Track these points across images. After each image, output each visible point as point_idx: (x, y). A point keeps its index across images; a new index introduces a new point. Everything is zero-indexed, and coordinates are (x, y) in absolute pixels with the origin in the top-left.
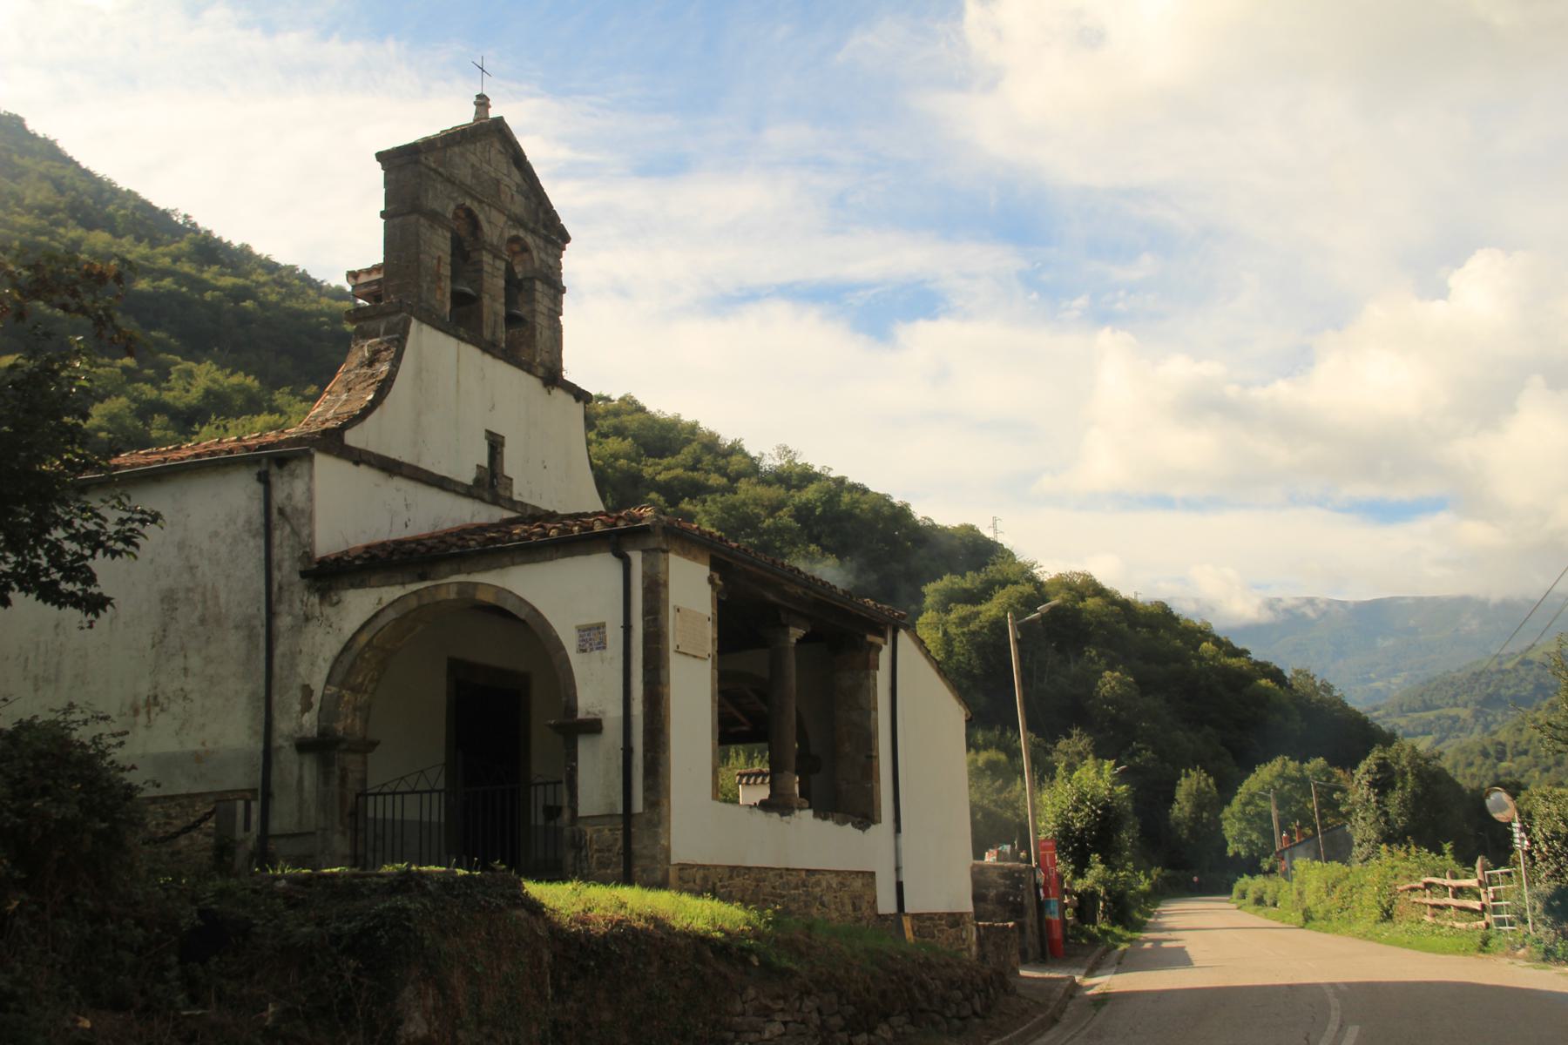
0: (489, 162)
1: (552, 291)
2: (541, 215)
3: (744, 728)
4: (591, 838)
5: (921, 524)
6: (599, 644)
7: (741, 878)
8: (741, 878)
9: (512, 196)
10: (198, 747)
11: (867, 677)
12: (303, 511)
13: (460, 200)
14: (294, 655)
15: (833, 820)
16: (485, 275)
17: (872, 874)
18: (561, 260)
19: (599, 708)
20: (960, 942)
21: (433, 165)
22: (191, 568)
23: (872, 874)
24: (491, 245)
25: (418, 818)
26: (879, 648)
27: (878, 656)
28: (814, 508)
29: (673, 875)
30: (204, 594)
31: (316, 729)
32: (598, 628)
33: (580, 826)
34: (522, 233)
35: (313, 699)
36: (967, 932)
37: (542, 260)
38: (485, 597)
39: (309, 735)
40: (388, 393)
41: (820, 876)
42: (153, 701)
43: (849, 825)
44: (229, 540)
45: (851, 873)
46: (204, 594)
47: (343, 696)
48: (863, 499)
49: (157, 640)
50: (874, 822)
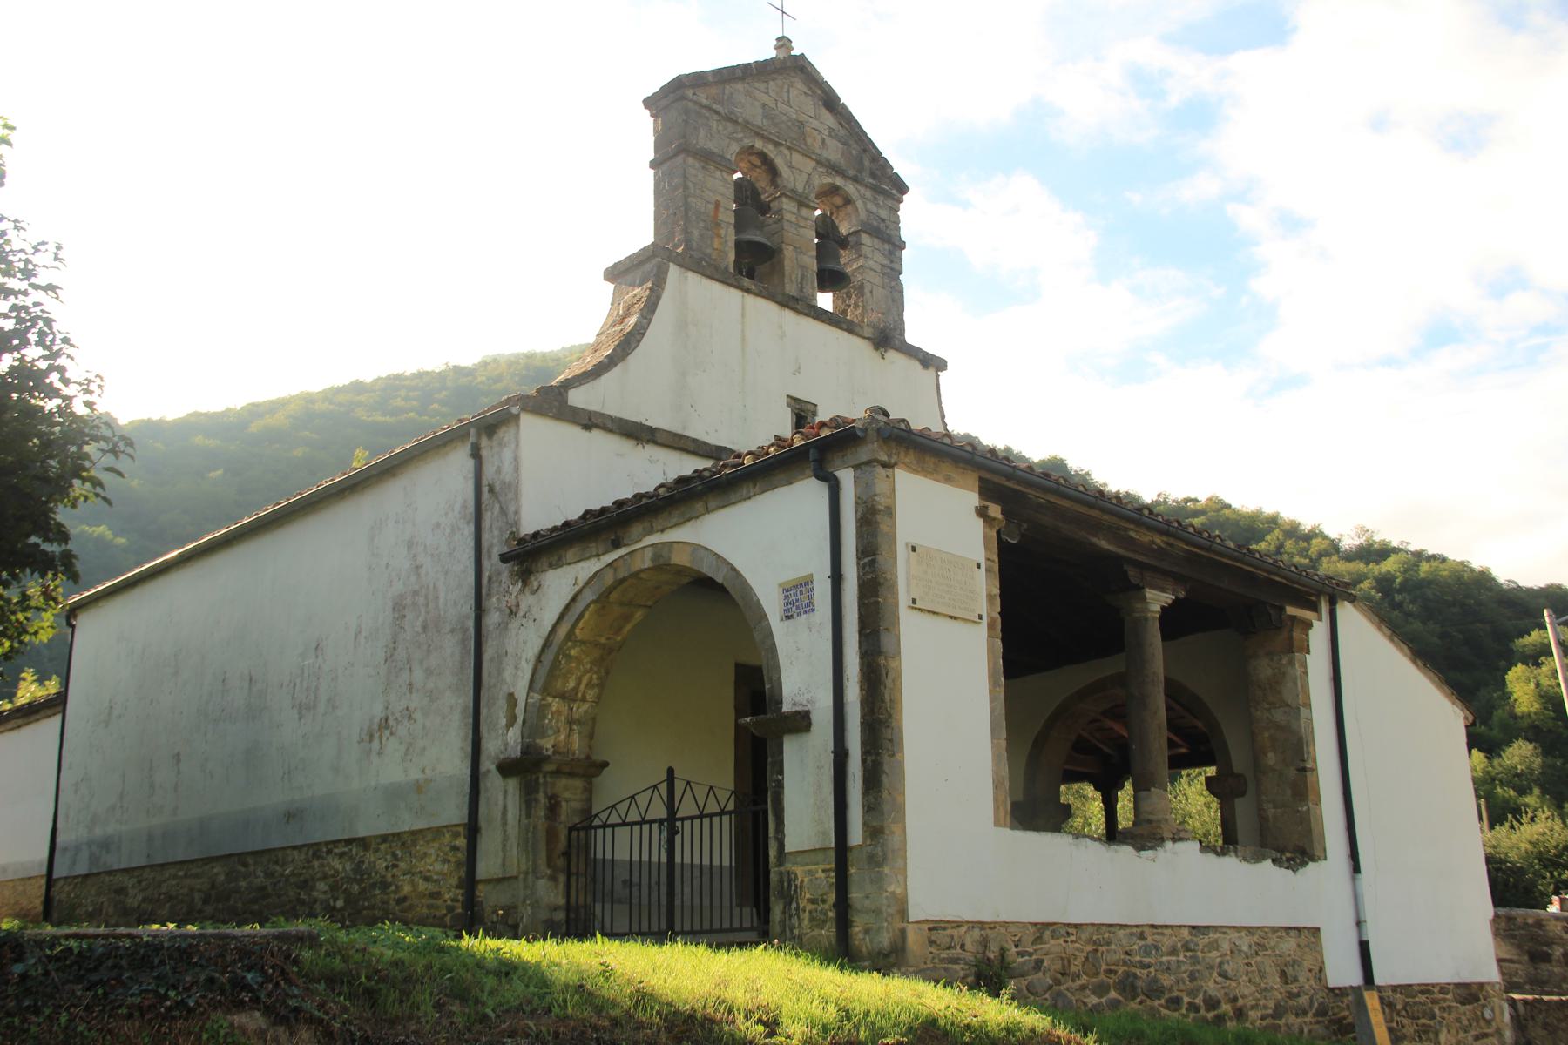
0: (788, 103)
1: (886, 246)
2: (867, 163)
3: (1183, 750)
4: (802, 881)
5: (1505, 587)
6: (808, 605)
7: (1061, 941)
8: (1061, 941)
9: (823, 141)
10: (420, 776)
11: (1291, 663)
12: (510, 485)
13: (747, 142)
14: (500, 657)
15: (1237, 856)
16: (786, 226)
17: (1316, 931)
18: (899, 213)
19: (807, 696)
20: (1482, 1023)
21: (705, 102)
22: (418, 567)
23: (1316, 931)
24: (794, 191)
25: (628, 858)
26: (1309, 625)
27: (1307, 635)
28: (1393, 579)
29: (914, 940)
30: (426, 597)
31: (519, 748)
32: (806, 584)
33: (788, 866)
34: (839, 181)
35: (517, 710)
36: (1493, 1010)
37: (869, 212)
38: (680, 559)
39: (513, 756)
40: (635, 348)
41: (1218, 935)
42: (385, 724)
43: (1268, 862)
44: (448, 530)
45: (1275, 930)
46: (426, 597)
47: (550, 705)
48: (1441, 566)
49: (389, 654)
50: (1313, 859)
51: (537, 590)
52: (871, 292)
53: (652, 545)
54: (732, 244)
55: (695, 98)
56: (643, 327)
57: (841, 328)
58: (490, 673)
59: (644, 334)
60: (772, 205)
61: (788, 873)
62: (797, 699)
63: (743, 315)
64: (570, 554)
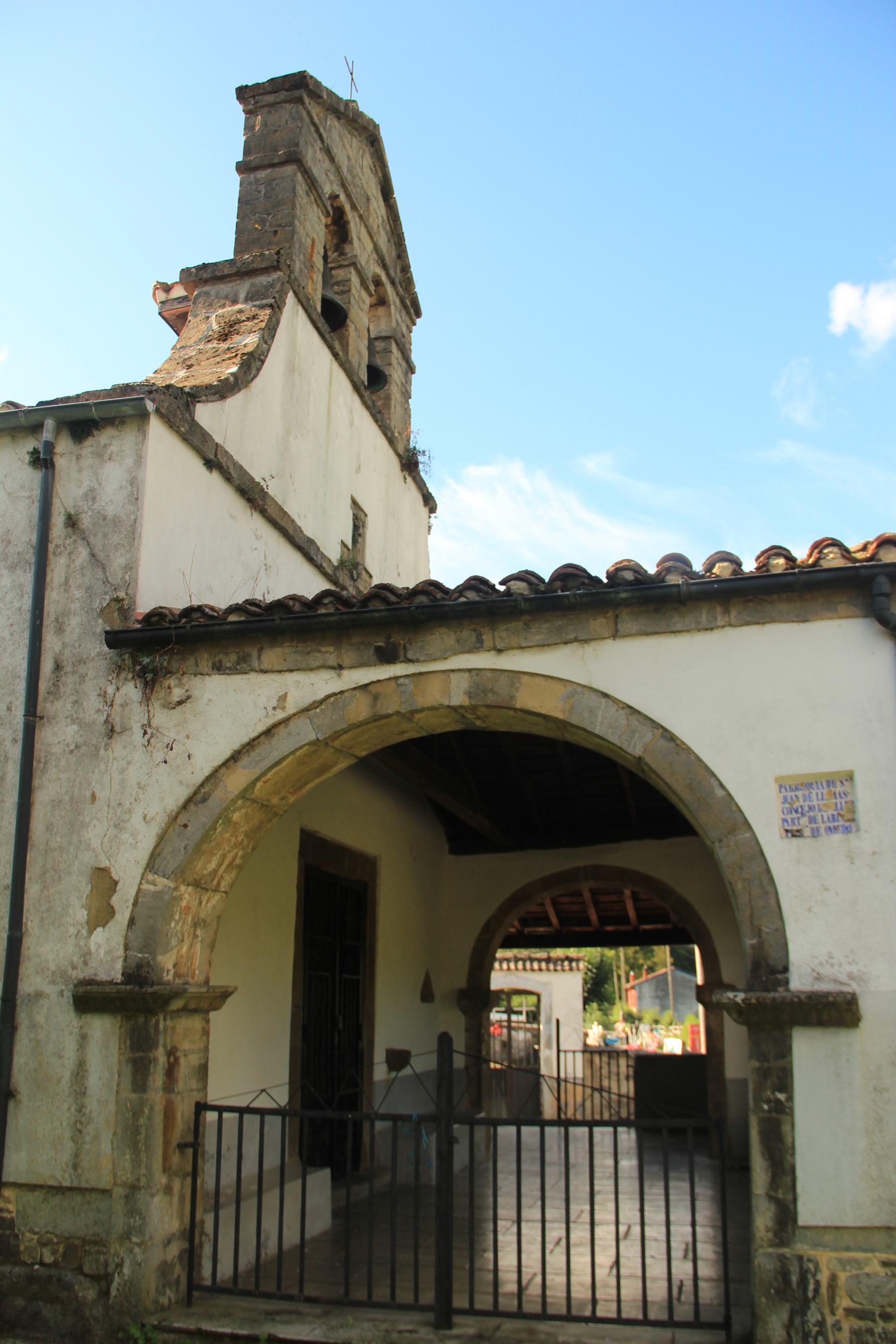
4: (833, 1278)
12: (116, 522)
19: (847, 968)
33: (801, 1248)
40: (255, 377)
51: (180, 703)
53: (470, 671)
57: (385, 435)
58: (49, 827)
59: (263, 362)
61: (800, 1258)
62: (825, 971)
63: (330, 384)
64: (271, 656)
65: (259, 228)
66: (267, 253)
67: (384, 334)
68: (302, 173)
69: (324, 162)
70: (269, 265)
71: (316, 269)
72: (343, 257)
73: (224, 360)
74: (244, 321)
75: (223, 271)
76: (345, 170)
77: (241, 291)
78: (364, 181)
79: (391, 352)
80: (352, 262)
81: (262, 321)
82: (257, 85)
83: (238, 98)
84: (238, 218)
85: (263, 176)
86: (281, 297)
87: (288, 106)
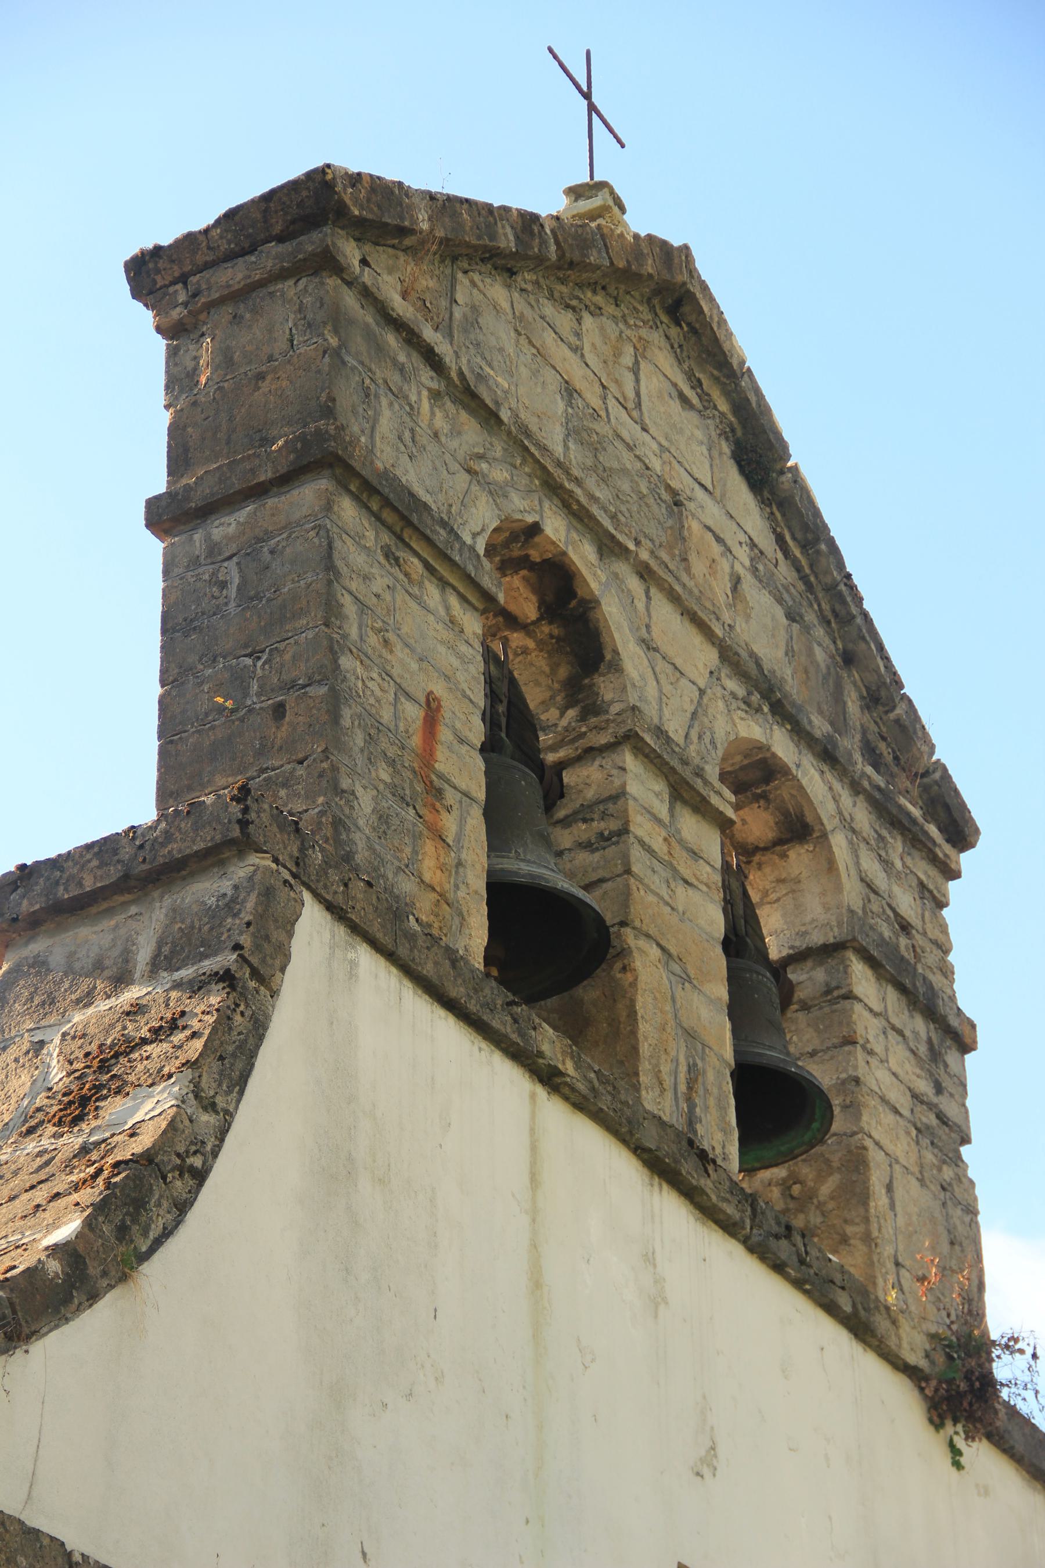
40: (167, 1233)
52: (889, 1188)
54: (478, 883)
55: (367, 277)
56: (198, 1146)
57: (830, 1308)
59: (200, 1176)
60: (568, 777)
63: (534, 1180)
65: (229, 704)
66: (209, 800)
67: (817, 938)
68: (356, 498)
69: (456, 432)
70: (218, 838)
71: (451, 797)
72: (593, 720)
73: (57, 1196)
74: (144, 1041)
75: (80, 884)
76: (554, 437)
77: (141, 939)
78: (649, 448)
79: (850, 996)
80: (622, 731)
81: (195, 1035)
82: (189, 240)
83: (136, 294)
84: (163, 683)
85: (231, 530)
86: (262, 938)
87: (289, 288)
